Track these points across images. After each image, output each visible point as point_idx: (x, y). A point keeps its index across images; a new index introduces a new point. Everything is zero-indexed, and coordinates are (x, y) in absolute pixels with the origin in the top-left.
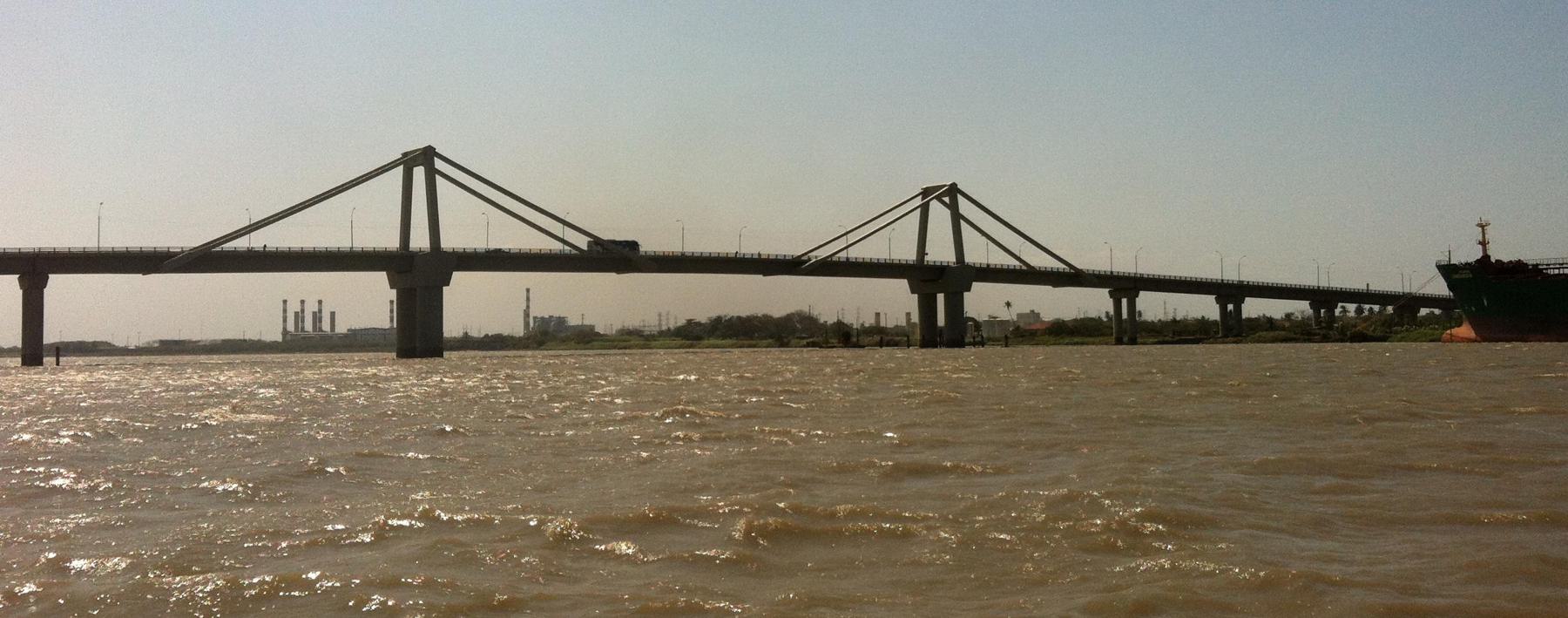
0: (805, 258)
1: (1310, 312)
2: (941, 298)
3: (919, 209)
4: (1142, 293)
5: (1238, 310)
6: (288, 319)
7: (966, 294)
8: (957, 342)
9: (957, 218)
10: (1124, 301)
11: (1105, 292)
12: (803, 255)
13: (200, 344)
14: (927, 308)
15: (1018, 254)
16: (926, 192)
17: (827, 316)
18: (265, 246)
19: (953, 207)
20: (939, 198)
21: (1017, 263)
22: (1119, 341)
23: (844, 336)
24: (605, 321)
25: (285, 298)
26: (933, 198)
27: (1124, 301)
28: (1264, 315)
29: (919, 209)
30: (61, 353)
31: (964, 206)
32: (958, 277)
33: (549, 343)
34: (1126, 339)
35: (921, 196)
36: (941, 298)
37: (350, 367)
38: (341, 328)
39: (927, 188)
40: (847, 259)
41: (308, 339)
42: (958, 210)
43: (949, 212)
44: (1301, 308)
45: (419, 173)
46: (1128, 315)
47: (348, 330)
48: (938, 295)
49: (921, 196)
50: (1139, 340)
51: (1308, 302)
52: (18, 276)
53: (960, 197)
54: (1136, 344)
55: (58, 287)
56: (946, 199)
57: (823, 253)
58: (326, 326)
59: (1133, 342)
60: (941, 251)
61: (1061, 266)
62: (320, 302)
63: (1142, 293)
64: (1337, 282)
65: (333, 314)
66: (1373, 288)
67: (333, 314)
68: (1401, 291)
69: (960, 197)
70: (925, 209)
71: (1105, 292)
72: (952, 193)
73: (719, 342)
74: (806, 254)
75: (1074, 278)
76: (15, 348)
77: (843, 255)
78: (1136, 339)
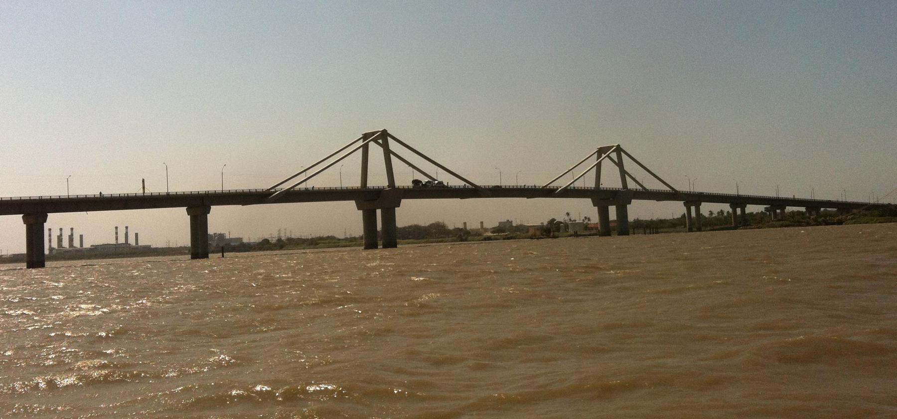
0: (273, 190)
1: (731, 210)
2: (379, 212)
3: (361, 149)
4: (703, 204)
5: (743, 211)
6: (52, 240)
7: (208, 215)
8: (390, 243)
9: (388, 153)
10: (693, 208)
11: (681, 203)
12: (271, 188)
13: (3, 257)
14: (604, 213)
15: (641, 182)
16: (365, 137)
17: (473, 225)
18: (101, 193)
19: (385, 146)
20: (375, 141)
21: (668, 189)
22: (691, 230)
23: (463, 235)
24: (251, 236)
25: (567, 212)
26: (612, 152)
27: (693, 208)
28: (638, 219)
29: (361, 149)
30: (224, 250)
31: (393, 145)
32: (622, 197)
33: (286, 246)
34: (694, 229)
35: (362, 140)
36: (379, 212)
37: (345, 253)
38: (87, 245)
39: (601, 148)
40: (574, 187)
41: (78, 251)
42: (389, 148)
43: (390, 149)
44: (726, 208)
45: (376, 151)
46: (696, 214)
47: (92, 246)
48: (692, 207)
49: (362, 140)
50: (702, 229)
51: (729, 204)
52: (22, 215)
53: (389, 139)
54: (692, 231)
55: (55, 222)
56: (380, 141)
57: (286, 186)
58: (77, 244)
59: (699, 230)
60: (378, 179)
61: (668, 189)
62: (61, 229)
63: (703, 204)
64: (744, 192)
65: (81, 236)
66: (796, 197)
67: (81, 236)
68: (775, 196)
69: (389, 139)
70: (365, 148)
71: (681, 203)
72: (383, 137)
73: (416, 241)
74: (569, 185)
75: (674, 195)
76: (185, 248)
77: (302, 186)
78: (692, 229)
